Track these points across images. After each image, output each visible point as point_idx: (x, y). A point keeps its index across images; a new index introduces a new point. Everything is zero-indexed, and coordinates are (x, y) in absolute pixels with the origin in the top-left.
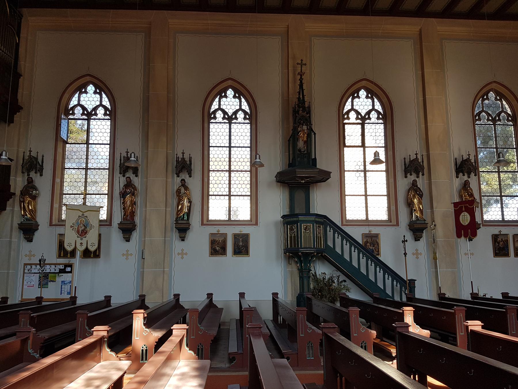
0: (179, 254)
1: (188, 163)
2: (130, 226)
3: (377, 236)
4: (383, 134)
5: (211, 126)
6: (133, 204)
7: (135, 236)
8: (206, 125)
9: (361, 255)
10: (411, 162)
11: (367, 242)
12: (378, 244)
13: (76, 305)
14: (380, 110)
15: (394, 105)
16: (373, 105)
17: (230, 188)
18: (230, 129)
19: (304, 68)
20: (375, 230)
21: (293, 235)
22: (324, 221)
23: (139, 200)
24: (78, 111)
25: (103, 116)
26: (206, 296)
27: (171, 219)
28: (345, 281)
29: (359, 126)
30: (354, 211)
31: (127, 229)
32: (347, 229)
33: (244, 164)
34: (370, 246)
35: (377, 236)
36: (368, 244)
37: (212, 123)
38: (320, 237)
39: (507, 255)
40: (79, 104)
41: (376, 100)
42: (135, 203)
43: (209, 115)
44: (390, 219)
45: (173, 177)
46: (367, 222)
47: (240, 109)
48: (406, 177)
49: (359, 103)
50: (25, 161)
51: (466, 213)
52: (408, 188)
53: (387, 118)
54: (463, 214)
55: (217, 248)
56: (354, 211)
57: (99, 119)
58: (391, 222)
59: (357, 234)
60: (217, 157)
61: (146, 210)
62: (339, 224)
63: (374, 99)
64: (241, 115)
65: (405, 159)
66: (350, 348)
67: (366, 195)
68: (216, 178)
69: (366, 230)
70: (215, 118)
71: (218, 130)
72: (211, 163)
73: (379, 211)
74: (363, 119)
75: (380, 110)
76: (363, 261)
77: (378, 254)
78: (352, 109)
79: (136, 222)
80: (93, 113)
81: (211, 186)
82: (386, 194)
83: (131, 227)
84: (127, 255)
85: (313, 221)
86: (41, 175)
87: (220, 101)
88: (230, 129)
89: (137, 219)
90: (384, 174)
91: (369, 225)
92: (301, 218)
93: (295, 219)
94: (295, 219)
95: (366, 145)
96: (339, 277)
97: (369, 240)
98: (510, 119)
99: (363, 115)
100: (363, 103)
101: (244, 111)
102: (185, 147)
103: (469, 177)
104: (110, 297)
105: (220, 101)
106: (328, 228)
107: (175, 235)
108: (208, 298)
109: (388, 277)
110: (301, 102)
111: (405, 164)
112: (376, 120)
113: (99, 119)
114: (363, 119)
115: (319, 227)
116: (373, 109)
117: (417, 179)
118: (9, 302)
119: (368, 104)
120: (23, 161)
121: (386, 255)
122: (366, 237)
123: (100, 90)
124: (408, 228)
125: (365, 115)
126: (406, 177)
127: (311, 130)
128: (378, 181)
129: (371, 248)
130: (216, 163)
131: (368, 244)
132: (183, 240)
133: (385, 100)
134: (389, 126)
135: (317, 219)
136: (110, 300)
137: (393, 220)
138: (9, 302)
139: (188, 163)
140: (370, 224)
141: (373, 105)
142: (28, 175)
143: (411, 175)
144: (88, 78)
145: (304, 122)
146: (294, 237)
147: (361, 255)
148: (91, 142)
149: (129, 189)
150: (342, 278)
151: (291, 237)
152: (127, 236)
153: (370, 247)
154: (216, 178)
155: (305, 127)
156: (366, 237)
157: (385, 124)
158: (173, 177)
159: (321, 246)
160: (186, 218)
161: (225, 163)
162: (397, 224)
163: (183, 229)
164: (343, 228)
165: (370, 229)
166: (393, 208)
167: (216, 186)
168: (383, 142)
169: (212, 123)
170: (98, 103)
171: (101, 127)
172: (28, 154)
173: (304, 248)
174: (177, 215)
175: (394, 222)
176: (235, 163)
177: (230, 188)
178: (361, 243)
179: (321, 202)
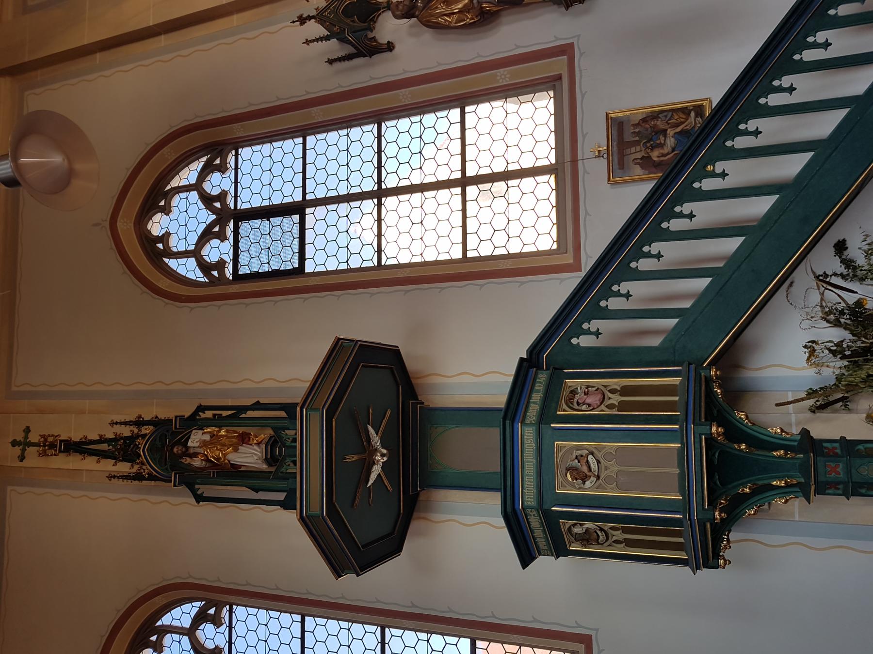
3: (616, 125)
4: (266, 148)
9: (707, 184)
10: (335, 33)
11: (646, 163)
12: (654, 116)
14: (197, 166)
15: (178, 123)
16: (187, 188)
19: (34, 437)
20: (594, 136)
21: (618, 535)
22: (545, 363)
25: (224, 628)
28: (840, 247)
29: (245, 227)
30: (523, 220)
32: (593, 248)
34: (661, 146)
35: (616, 125)
36: (655, 155)
38: (625, 391)
41: (175, 183)
44: (554, 88)
46: (565, 171)
48: (390, 47)
49: (182, 233)
52: (428, 35)
53: (216, 140)
56: (523, 220)
57: (230, 643)
58: (559, 78)
59: (614, 204)
62: (571, 282)
63: (173, 189)
67: (464, 182)
68: (256, 186)
69: (594, 171)
72: (355, 263)
73: (519, 128)
75: (197, 166)
76: (739, 173)
77: (699, 109)
78: (195, 253)
85: (539, 435)
91: (574, 161)
92: (528, 494)
93: (535, 522)
94: (535, 522)
95: (298, 197)
96: (822, 279)
97: (637, 152)
99: (214, 217)
100: (181, 222)
106: (584, 341)
109: (815, 45)
110: (122, 449)
111: (349, 57)
112: (227, 174)
113: (230, 643)
114: (227, 217)
115: (569, 402)
116: (197, 187)
121: (706, 77)
122: (622, 165)
124: (578, 7)
125: (214, 210)
126: (390, 47)
127: (193, 421)
128: (421, 144)
129: (671, 142)
131: (655, 155)
133: (169, 154)
134: (238, 130)
135: (534, 410)
137: (548, 73)
140: (568, 157)
141: (187, 188)
145: (178, 443)
146: (625, 531)
147: (707, 184)
150: (825, 259)
151: (629, 543)
153: (674, 152)
154: (404, 241)
155: (196, 439)
156: (622, 165)
157: (237, 144)
159: (670, 406)
162: (566, 50)
164: (588, 261)
166: (503, 77)
167: (277, 183)
168: (288, 144)
173: (684, 489)
175: (559, 65)
178: (646, 188)
179: (473, 364)
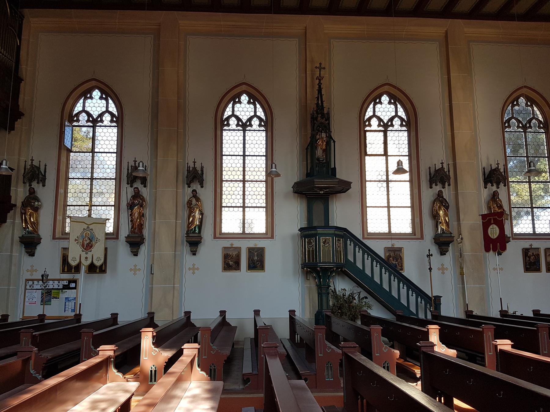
0: (190, 269)
1: (200, 172)
2: (139, 240)
3: (400, 250)
4: (406, 142)
5: (225, 133)
6: (141, 216)
7: (144, 250)
8: (219, 132)
9: (383, 270)
10: (437, 171)
11: (389, 256)
12: (401, 259)
13: (80, 323)
14: (404, 116)
15: (418, 111)
16: (396, 111)
17: (244, 199)
18: (244, 136)
19: (323, 72)
20: (398, 244)
21: (311, 249)
22: (344, 234)
23: (147, 212)
24: (83, 117)
25: (109, 123)
26: (219, 314)
27: (181, 232)
28: (366, 298)
29: (382, 134)
30: (376, 223)
31: (135, 243)
32: (368, 243)
33: (259, 173)
34: (393, 260)
35: (400, 250)
36: (391, 259)
37: (225, 130)
38: (340, 251)
39: (538, 270)
40: (84, 111)
41: (399, 106)
42: (143, 215)
43: (222, 121)
44: (414, 232)
45: (184, 187)
46: (389, 236)
47: (255, 115)
48: (431, 187)
49: (382, 110)
50: (26, 170)
51: (495, 226)
52: (433, 199)
53: (411, 125)
54: (491, 227)
55: (231, 262)
56: (376, 223)
57: (105, 126)
58: (415, 235)
59: (379, 248)
60: (231, 167)
61: (155, 223)
62: (360, 237)
63: (397, 105)
64: (255, 122)
65: (430, 168)
66: (372, 368)
67: (389, 207)
68: (229, 189)
69: (388, 244)
70: (228, 125)
71: (232, 138)
72: (224, 173)
73: (403, 223)
74: (386, 126)
75: (404, 116)
76: (386, 276)
77: (402, 269)
78: (374, 115)
79: (144, 235)
80: (99, 119)
81: (224, 197)
82: (410, 205)
83: (139, 240)
84: (135, 270)
85: (333, 234)
86: (44, 186)
87: (233, 107)
88: (244, 136)
89: (146, 232)
90: (408, 184)
91: (391, 239)
92: (320, 231)
93: (313, 232)
94: (313, 232)
95: (389, 154)
96: (360, 293)
97: (392, 254)
98: (542, 126)
99: (386, 122)
100: (385, 109)
101: (259, 118)
102: (196, 155)
103: (498, 188)
104: (117, 314)
105: (233, 107)
106: (349, 242)
107: (186, 249)
108: (221, 315)
109: (412, 293)
110: (320, 108)
111: (430, 174)
112: (399, 127)
113: (105, 126)
114: (386, 126)
115: (338, 240)
116: (396, 115)
117: (443, 190)
118: (10, 320)
119: (391, 110)
120: (25, 171)
121: (410, 270)
122: (389, 250)
123: (106, 95)
124: (433, 241)
125: (388, 122)
126: (431, 187)
127: (330, 138)
128: (402, 191)
129: (394, 262)
130: (229, 173)
131: (391, 259)
132: (194, 254)
133: (409, 106)
134: (413, 134)
135: (337, 232)
136: (117, 318)
137: (418, 232)
138: (10, 320)
139: (200, 172)
140: (393, 237)
141: (396, 111)
142: (30, 185)
143: (436, 185)
144: (94, 83)
145: (322, 129)
146: (313, 251)
147: (383, 270)
148: (96, 150)
149: (137, 200)
150: (363, 294)
151: (309, 251)
152: (135, 250)
153: (392, 262)
154: (229, 189)
155: (324, 135)
156: (389, 250)
157: (409, 131)
158: (184, 187)
159: (341, 261)
160: (197, 231)
161: (239, 173)
162: (422, 238)
163: (194, 242)
164: (364, 241)
165: (393, 242)
166: (417, 220)
167: (229, 197)
168: (407, 150)
169: (225, 130)
170: (104, 109)
171: (107, 134)
172: (30, 163)
173: (323, 263)
174: (188, 227)
175: (418, 235)
176: (250, 173)
177: (244, 199)
178: (383, 257)
179: (340, 214)
